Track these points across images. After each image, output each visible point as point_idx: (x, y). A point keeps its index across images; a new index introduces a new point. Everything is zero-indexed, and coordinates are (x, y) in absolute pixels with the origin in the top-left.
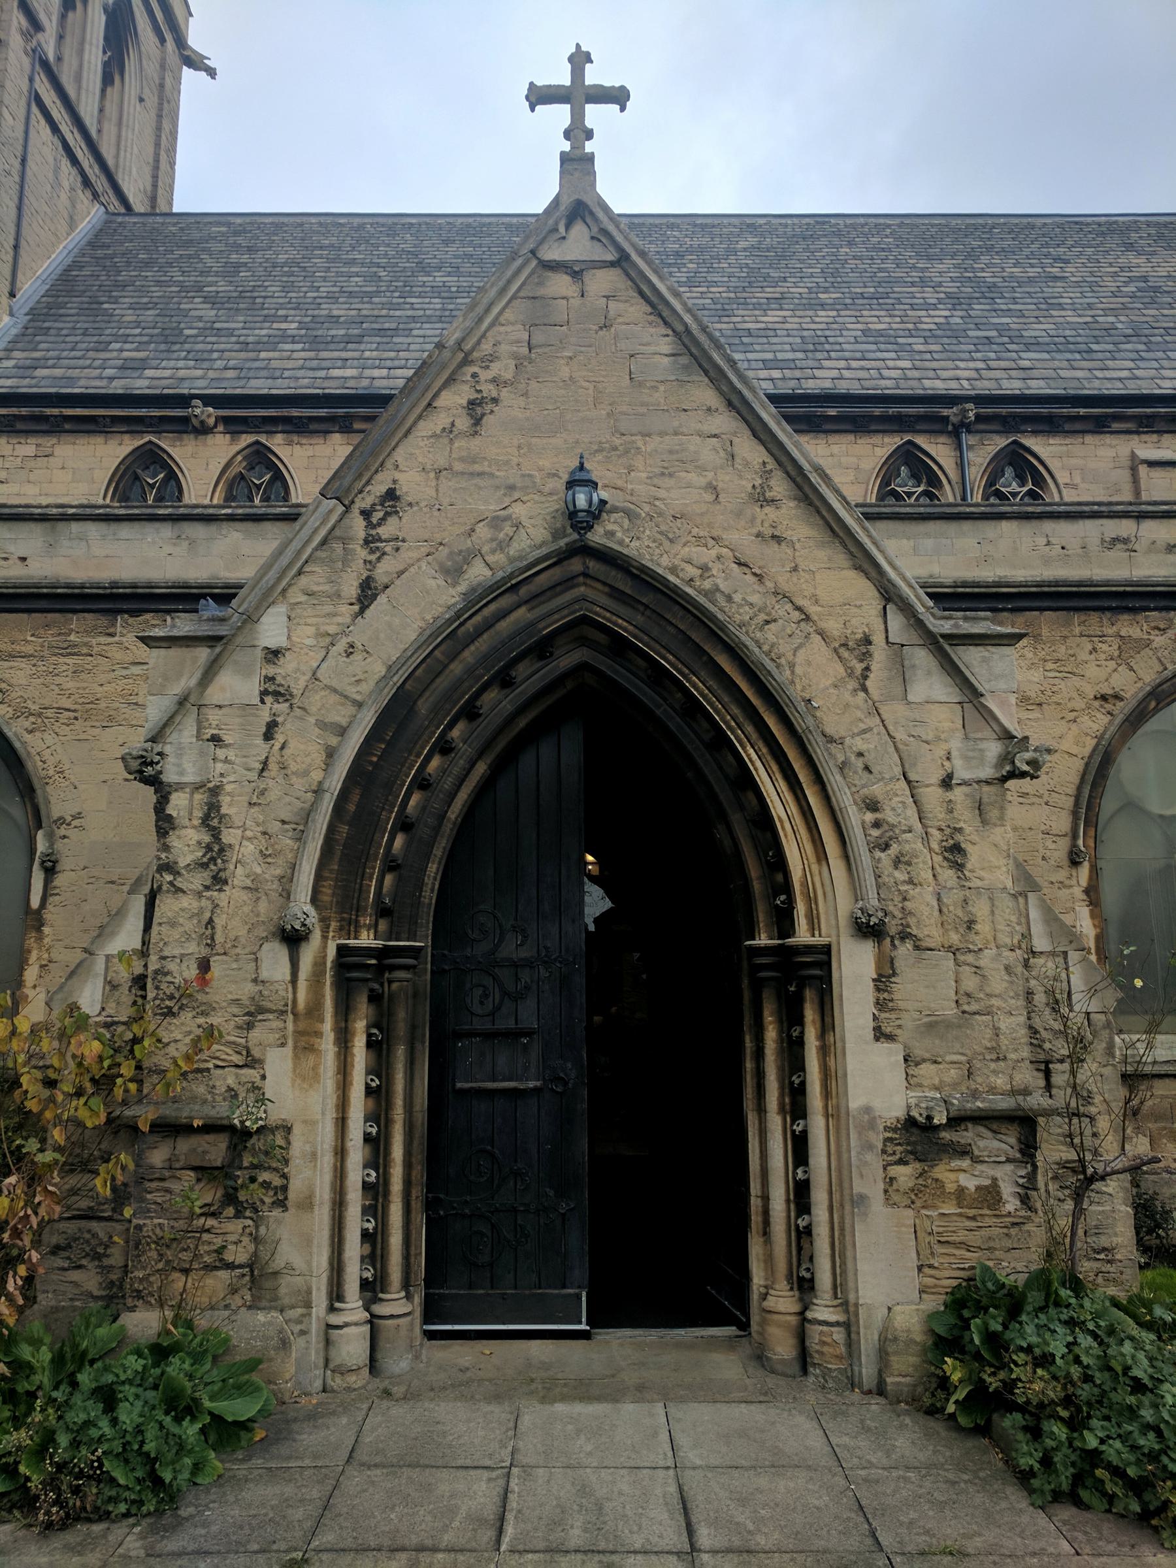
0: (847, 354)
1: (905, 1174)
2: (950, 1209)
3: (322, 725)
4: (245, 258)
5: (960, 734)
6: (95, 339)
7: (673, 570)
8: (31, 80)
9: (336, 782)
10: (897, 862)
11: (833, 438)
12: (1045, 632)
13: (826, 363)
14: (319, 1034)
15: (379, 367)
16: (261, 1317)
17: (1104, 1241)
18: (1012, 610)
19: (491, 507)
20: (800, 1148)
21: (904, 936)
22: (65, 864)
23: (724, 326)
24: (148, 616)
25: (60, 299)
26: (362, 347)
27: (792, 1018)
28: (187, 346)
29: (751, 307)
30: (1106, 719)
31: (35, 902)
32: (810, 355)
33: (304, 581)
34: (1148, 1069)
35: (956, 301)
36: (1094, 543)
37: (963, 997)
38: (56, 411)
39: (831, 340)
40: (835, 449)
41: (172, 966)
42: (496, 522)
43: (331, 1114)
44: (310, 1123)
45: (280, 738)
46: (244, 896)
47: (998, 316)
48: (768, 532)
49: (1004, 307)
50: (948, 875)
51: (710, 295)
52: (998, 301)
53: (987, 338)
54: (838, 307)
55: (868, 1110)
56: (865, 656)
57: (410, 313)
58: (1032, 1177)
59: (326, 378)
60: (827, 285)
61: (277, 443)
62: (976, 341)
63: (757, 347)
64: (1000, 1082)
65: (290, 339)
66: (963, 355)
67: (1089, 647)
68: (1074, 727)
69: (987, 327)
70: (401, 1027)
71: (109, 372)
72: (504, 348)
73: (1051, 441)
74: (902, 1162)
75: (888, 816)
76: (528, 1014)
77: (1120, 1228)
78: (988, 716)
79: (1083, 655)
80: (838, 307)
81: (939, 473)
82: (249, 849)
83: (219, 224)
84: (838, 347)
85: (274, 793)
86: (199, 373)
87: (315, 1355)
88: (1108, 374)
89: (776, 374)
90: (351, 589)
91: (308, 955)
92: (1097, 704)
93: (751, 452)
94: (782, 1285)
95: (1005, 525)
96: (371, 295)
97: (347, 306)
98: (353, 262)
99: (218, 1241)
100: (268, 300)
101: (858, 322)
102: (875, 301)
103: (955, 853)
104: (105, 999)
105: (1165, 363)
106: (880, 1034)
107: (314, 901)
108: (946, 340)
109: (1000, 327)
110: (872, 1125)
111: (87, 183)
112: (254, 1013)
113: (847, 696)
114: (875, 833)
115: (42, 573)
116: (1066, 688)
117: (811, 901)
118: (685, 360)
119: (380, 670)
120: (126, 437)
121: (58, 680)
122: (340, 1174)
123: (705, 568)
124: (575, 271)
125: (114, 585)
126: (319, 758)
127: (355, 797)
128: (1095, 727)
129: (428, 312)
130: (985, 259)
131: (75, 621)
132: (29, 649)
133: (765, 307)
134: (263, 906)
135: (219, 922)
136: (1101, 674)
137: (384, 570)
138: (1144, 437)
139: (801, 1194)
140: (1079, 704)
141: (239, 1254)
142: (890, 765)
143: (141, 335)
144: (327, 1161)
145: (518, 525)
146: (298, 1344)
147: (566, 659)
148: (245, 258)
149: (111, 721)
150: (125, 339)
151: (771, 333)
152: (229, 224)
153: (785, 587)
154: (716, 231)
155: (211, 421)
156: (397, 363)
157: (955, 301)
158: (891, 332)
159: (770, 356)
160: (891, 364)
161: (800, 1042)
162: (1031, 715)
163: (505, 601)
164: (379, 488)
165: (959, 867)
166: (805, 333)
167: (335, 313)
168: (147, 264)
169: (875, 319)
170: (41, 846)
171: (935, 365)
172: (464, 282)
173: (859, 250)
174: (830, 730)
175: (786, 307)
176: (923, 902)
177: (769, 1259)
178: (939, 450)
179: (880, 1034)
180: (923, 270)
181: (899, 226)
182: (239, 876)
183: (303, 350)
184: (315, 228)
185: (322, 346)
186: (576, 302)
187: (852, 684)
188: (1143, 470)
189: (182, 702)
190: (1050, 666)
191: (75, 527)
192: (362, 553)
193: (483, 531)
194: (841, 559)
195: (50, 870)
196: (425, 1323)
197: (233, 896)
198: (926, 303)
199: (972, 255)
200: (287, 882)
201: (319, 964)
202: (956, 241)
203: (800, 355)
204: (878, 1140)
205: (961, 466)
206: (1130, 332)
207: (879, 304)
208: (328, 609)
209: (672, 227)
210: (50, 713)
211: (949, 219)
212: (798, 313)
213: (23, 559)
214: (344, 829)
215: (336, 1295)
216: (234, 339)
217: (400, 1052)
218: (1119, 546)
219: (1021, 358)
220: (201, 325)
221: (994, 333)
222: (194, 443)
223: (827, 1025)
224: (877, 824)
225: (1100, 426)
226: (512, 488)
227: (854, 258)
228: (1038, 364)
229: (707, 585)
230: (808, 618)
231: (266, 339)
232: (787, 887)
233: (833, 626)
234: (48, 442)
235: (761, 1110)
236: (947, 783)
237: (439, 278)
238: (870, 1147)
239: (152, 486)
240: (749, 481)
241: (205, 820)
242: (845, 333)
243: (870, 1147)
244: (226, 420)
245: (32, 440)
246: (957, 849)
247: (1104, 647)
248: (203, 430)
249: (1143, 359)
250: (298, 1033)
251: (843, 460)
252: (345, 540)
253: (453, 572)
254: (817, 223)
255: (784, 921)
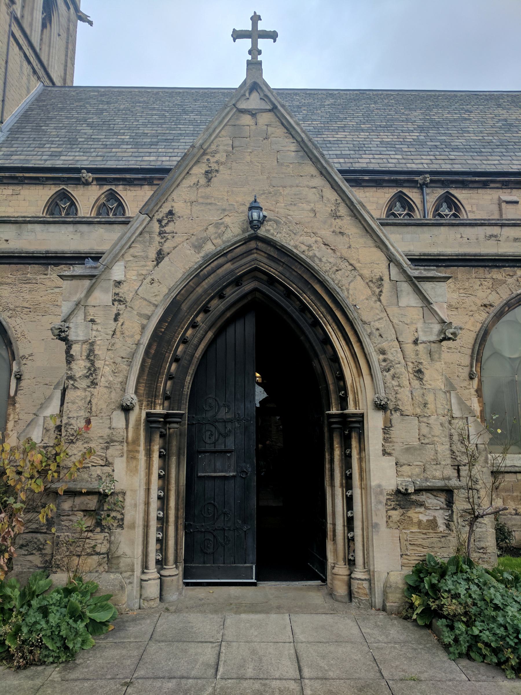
0: (373, 152)
1: (396, 514)
2: (415, 529)
3: (140, 315)
4: (106, 107)
5: (422, 321)
6: (39, 142)
7: (296, 247)
8: (10, 26)
9: (145, 340)
10: (393, 377)
11: (367, 189)
12: (459, 276)
13: (364, 156)
14: (138, 452)
15: (165, 156)
16: (112, 576)
17: (482, 544)
18: (445, 266)
19: (215, 218)
20: (349, 502)
21: (396, 409)
22: (25, 376)
23: (319, 139)
24: (62, 266)
25: (23, 125)
26: (158, 147)
27: (346, 445)
28: (80, 146)
29: (331, 131)
30: (485, 315)
31: (12, 393)
32: (357, 152)
33: (132, 250)
34: (503, 469)
35: (422, 129)
36: (482, 237)
37: (421, 436)
38: (21, 175)
39: (366, 146)
40: (367, 194)
41: (73, 421)
42: (217, 225)
43: (143, 487)
44: (134, 491)
45: (121, 321)
46: (105, 390)
47: (441, 136)
48: (338, 230)
49: (443, 132)
50: (416, 383)
51: (313, 125)
52: (440, 129)
53: (436, 145)
54: (369, 131)
55: (379, 486)
56: (380, 286)
57: (179, 132)
58: (451, 516)
59: (142, 161)
60: (365, 121)
61: (120, 189)
62: (430, 147)
63: (333, 149)
64: (438, 474)
65: (126, 143)
66: (425, 153)
67: (479, 283)
68: (472, 318)
69: (436, 141)
70: (174, 449)
71: (45, 157)
72: (221, 148)
73: (463, 192)
74: (394, 509)
75: (390, 356)
76: (230, 443)
77: (489, 539)
78: (434, 313)
79: (476, 287)
80: (369, 131)
81: (414, 205)
82: (107, 369)
83: (94, 91)
84: (369, 149)
85: (117, 346)
86: (85, 158)
87: (136, 592)
88: (489, 162)
89: (342, 160)
90: (153, 255)
91: (133, 416)
92: (482, 308)
93: (330, 195)
94: (341, 562)
95: (442, 228)
96: (162, 124)
97: (151, 129)
98: (154, 109)
99: (93, 543)
100: (116, 126)
101: (378, 138)
102: (386, 129)
103: (419, 373)
104: (44, 435)
105: (514, 158)
106: (385, 453)
107: (136, 392)
108: (417, 146)
109: (441, 141)
110: (381, 493)
111: (35, 72)
112: (109, 442)
113: (372, 303)
114: (384, 364)
115: (15, 247)
116: (469, 301)
117: (355, 394)
118: (301, 154)
119: (165, 290)
120: (53, 186)
121: (22, 294)
122: (147, 513)
123: (310, 246)
124: (253, 114)
125: (47, 252)
126: (138, 329)
127: (154, 347)
128: (481, 318)
129: (187, 132)
130: (435, 110)
131: (30, 268)
132: (9, 281)
133: (337, 131)
134: (113, 395)
135: (94, 402)
136: (484, 295)
137: (167, 247)
138: (504, 190)
139: (350, 522)
140: (474, 308)
141: (102, 548)
142: (390, 334)
143: (59, 141)
144: (141, 507)
145: (227, 227)
146: (128, 588)
147: (248, 286)
148: (106, 107)
149: (45, 313)
150: (52, 142)
151: (340, 142)
152: (98, 91)
153: (345, 255)
154: (316, 96)
155: (90, 180)
156: (173, 154)
157: (421, 129)
158: (393, 142)
159: (339, 152)
160: (392, 156)
161: (350, 456)
162: (453, 313)
163: (221, 260)
164: (165, 210)
165: (421, 379)
166: (355, 143)
167: (146, 132)
168: (62, 109)
169: (386, 137)
170: (15, 368)
171: (412, 157)
172: (203, 118)
173: (379, 106)
174: (364, 318)
175: (346, 131)
176: (404, 394)
177: (335, 551)
178: (413, 195)
179: (385, 453)
180: (407, 115)
181: (398, 95)
182: (102, 382)
183: (132, 148)
184: (137, 93)
185: (140, 147)
186: (253, 127)
187: (374, 298)
188: (504, 205)
189: (78, 304)
190: (461, 291)
191: (30, 226)
192: (158, 239)
193: (211, 229)
194: (370, 242)
195: (19, 379)
196: (184, 579)
197: (100, 391)
198: (409, 130)
199: (429, 108)
200: (124, 384)
201: (138, 421)
202: (422, 102)
203: (352, 152)
204: (383, 499)
205: (423, 202)
206: (499, 143)
207: (388, 130)
208: (143, 263)
209: (296, 94)
210: (19, 309)
211: (419, 92)
212: (352, 134)
213: (7, 241)
214: (149, 361)
215: (145, 566)
216: (100, 143)
217: (174, 459)
218: (493, 238)
219: (450, 155)
220: (86, 136)
221: (438, 143)
222: (82, 189)
223: (362, 449)
224: (385, 360)
225: (485, 185)
226: (224, 210)
227: (377, 109)
228: (457, 157)
229: (311, 254)
230: (355, 269)
231: (115, 143)
232: (345, 388)
233: (366, 272)
234: (18, 188)
235: (332, 486)
236: (416, 342)
237: (192, 116)
238: (381, 502)
239: (64, 208)
240: (330, 208)
241: (88, 356)
242: (372, 142)
243: (381, 502)
244: (97, 179)
245: (11, 187)
246: (420, 371)
247: (486, 283)
248: (87, 184)
249: (504, 156)
250: (129, 451)
251: (371, 199)
252: (150, 233)
253: (198, 247)
254: (361, 93)
255: (343, 402)
